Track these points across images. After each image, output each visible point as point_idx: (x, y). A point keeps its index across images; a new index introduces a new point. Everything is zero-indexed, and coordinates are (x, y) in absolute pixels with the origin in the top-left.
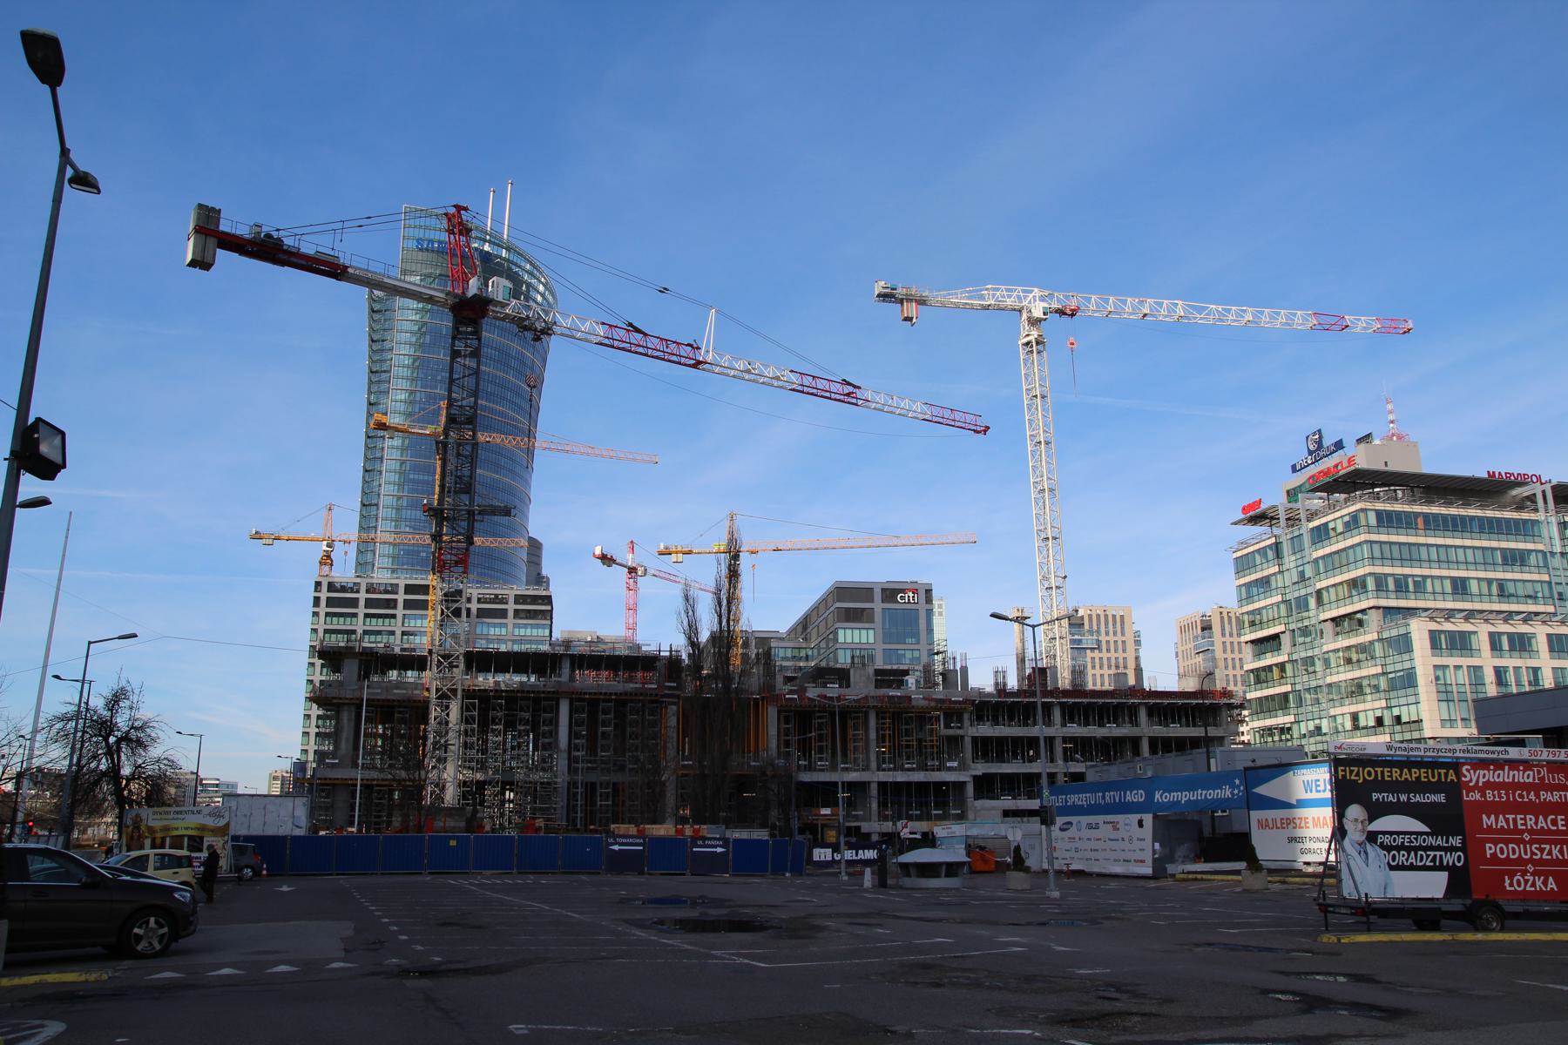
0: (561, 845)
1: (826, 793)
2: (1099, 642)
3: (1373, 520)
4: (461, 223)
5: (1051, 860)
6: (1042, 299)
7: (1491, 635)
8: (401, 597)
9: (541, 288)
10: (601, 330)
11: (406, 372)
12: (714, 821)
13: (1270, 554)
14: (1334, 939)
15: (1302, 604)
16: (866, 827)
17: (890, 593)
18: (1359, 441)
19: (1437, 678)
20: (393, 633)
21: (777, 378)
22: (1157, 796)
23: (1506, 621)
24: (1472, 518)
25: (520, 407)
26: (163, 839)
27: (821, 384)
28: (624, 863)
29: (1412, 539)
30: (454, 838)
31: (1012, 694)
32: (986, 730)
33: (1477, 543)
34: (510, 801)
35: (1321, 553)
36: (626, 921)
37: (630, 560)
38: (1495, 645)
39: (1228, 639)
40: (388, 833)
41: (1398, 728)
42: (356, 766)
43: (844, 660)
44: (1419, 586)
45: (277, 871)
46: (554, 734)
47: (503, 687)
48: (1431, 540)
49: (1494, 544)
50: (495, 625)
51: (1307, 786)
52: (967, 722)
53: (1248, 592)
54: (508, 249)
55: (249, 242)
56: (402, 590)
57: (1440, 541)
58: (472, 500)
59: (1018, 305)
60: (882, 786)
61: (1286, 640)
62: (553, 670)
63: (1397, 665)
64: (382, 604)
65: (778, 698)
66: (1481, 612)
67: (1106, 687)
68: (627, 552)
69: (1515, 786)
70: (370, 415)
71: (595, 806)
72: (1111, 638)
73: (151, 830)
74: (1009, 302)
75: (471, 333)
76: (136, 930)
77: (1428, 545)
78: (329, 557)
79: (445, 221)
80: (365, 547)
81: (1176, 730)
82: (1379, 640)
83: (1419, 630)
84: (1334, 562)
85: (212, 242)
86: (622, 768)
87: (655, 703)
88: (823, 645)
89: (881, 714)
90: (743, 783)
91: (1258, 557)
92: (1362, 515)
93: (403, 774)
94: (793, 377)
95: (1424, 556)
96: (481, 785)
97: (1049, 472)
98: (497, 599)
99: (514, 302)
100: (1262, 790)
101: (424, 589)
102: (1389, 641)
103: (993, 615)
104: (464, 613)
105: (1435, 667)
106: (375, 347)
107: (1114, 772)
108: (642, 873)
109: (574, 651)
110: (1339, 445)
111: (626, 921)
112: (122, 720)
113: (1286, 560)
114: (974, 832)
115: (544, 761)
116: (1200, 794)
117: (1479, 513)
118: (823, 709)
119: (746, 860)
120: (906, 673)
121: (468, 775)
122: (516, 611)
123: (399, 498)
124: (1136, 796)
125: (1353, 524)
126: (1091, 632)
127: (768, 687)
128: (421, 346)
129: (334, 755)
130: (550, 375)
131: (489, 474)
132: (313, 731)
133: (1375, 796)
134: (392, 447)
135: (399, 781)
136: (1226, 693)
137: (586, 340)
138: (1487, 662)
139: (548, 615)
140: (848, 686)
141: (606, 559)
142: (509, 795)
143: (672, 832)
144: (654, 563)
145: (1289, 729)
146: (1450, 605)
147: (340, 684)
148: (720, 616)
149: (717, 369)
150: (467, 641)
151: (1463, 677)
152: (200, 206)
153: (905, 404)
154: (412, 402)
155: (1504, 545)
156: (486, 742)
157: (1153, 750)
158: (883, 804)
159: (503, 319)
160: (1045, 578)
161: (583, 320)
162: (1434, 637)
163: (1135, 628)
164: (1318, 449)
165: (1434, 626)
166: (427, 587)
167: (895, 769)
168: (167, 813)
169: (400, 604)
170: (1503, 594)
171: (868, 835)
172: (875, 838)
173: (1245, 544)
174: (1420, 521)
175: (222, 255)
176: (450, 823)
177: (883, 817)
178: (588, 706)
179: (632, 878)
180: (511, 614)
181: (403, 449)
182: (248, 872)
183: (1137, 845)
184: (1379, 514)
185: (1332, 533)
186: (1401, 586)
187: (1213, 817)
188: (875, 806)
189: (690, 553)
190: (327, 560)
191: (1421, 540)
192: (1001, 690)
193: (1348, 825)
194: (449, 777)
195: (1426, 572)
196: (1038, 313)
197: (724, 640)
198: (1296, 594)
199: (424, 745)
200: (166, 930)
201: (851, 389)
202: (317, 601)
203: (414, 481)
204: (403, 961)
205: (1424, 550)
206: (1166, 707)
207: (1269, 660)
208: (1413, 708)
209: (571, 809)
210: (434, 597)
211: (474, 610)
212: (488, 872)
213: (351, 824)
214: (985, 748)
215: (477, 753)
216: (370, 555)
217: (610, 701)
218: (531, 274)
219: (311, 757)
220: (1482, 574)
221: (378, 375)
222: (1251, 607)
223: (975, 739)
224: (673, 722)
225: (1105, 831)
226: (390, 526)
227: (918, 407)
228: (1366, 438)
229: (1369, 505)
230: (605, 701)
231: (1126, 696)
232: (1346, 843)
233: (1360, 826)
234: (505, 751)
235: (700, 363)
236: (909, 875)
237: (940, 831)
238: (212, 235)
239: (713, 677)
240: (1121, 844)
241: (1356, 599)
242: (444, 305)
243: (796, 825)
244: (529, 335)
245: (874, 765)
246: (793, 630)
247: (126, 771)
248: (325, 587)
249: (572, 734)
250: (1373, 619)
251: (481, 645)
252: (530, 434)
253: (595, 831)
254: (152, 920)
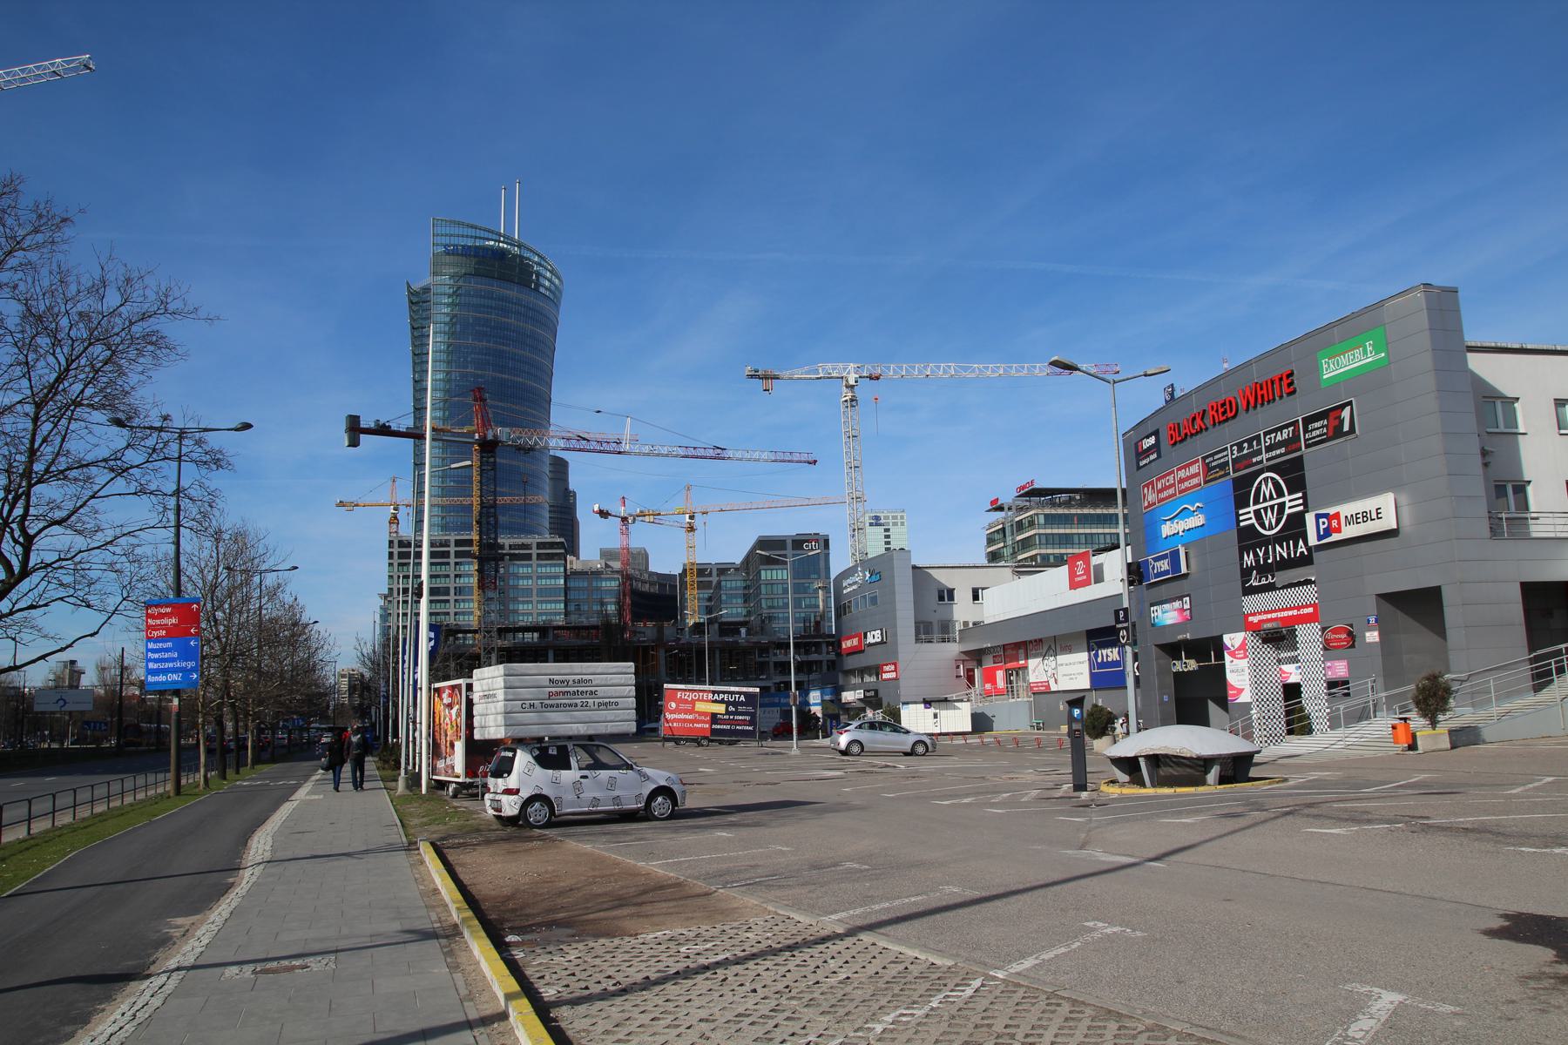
3: (1042, 520)
17: (799, 543)
37: (622, 512)
69: (685, 721)
89: (722, 651)
122: (539, 555)
128: (452, 334)
141: (604, 514)
154: (449, 381)
190: (394, 520)
196: (852, 382)
202: (391, 555)
218: (539, 264)
227: (765, 456)
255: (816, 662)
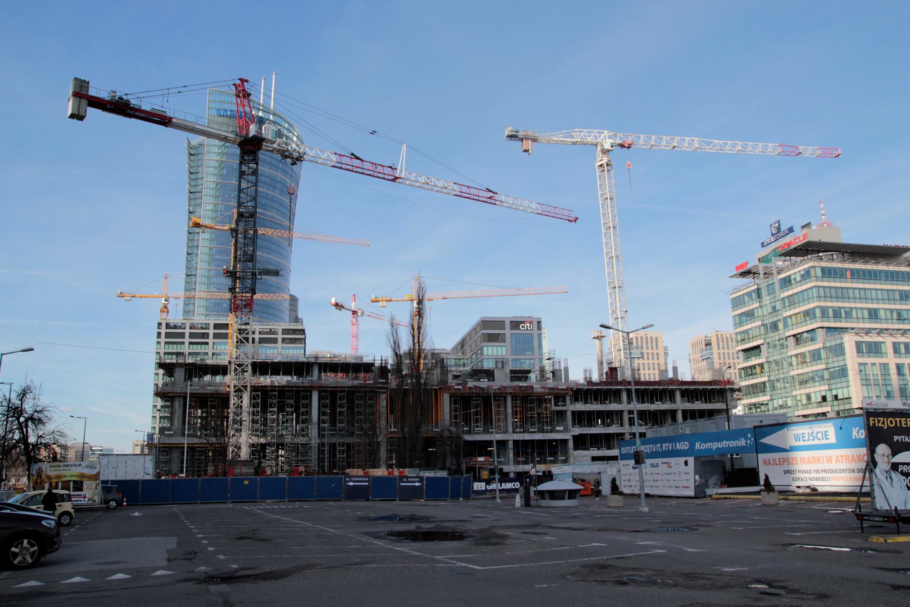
0: (318, 481)
1: (482, 448)
2: (642, 354)
3: (819, 273)
4: (244, 90)
5: (642, 488)
6: (610, 137)
7: (894, 344)
8: (211, 331)
9: (295, 139)
10: (334, 158)
11: (212, 192)
12: (411, 466)
13: (754, 296)
14: (882, 540)
15: (775, 327)
16: (506, 469)
17: (515, 324)
18: (803, 227)
19: (861, 371)
20: (207, 354)
21: (446, 188)
22: (697, 445)
23: (903, 335)
24: (881, 271)
25: (283, 213)
26: (57, 483)
27: (473, 191)
28: (357, 494)
29: (843, 285)
30: (247, 479)
31: (596, 384)
32: (580, 407)
33: (884, 287)
34: (282, 456)
35: (786, 294)
36: (367, 534)
38: (896, 350)
39: (721, 351)
40: (204, 477)
41: (836, 403)
42: (183, 435)
43: (488, 365)
44: (848, 314)
45: (134, 502)
46: (309, 413)
47: (276, 384)
48: (855, 285)
49: (895, 287)
50: (270, 348)
51: (797, 438)
52: (568, 402)
53: (740, 319)
54: (274, 115)
55: (108, 102)
56: (212, 327)
57: (861, 286)
58: (254, 266)
59: (595, 141)
60: (516, 442)
61: (764, 348)
62: (308, 373)
63: (835, 363)
64: (200, 336)
65: (449, 388)
66: (887, 330)
67: (657, 379)
68: (348, 305)
70: (190, 219)
71: (336, 459)
72: (650, 351)
73: (49, 478)
74: (589, 140)
75: (252, 160)
76: (13, 549)
77: (854, 289)
78: (166, 307)
79: (233, 88)
80: (189, 301)
81: (699, 405)
82: (824, 348)
83: (849, 341)
84: (792, 301)
85: (84, 102)
86: (352, 434)
87: (372, 393)
88: (474, 357)
89: (514, 397)
90: (430, 441)
91: (746, 298)
92: (812, 270)
93: (214, 440)
94: (456, 187)
95: (851, 295)
96: (264, 446)
97: (615, 245)
98: (271, 332)
99: (279, 140)
100: (767, 440)
101: (226, 326)
102: (830, 348)
103: (602, 326)
104: (250, 341)
105: (859, 364)
106: (193, 177)
107: (665, 431)
108: (368, 500)
109: (321, 361)
110: (791, 230)
111: (367, 534)
112: (28, 407)
113: (764, 299)
114: (578, 470)
115: (303, 430)
116: (724, 444)
117: (885, 268)
118: (478, 395)
119: (435, 491)
120: (529, 372)
121: (255, 440)
122: (283, 339)
123: (209, 270)
124: (683, 446)
125: (807, 275)
126: (637, 347)
127: (444, 382)
129: (169, 429)
130: (302, 174)
131: (265, 255)
132: (158, 415)
133: (896, 438)
134: (204, 238)
135: (211, 445)
136: (729, 382)
137: (326, 165)
138: (892, 360)
139: (303, 341)
140: (493, 380)
142: (281, 452)
143: (386, 473)
144: (368, 308)
145: (767, 404)
146: (867, 326)
147: (174, 384)
148: (413, 336)
149: (408, 182)
150: (253, 358)
151: (877, 371)
152: (76, 79)
153: (526, 203)
154: (216, 211)
155: (901, 288)
156: (266, 419)
157: (685, 418)
158: (516, 454)
159: (271, 151)
160: (614, 312)
161: (323, 152)
162: (858, 345)
163: (665, 344)
164: (778, 232)
165: (858, 339)
166: (228, 324)
167: (524, 432)
168: (59, 466)
169: (211, 336)
170: (900, 319)
171: (508, 474)
172: (512, 475)
173: (738, 289)
174: (848, 273)
175: (92, 112)
176: (244, 470)
177: (517, 463)
178: (330, 395)
179: (363, 503)
180: (280, 341)
181: (211, 240)
182: (113, 504)
183: (684, 477)
184: (823, 269)
185: (793, 282)
186: (837, 314)
187: (732, 458)
188: (511, 455)
189: (390, 301)
191: (849, 285)
192: (590, 383)
193: (878, 458)
194: (243, 441)
195: (852, 305)
196: (607, 146)
197: (416, 354)
198: (771, 320)
199: (227, 422)
200: (36, 548)
201: (491, 194)
202: (159, 334)
203: (216, 260)
204: (210, 569)
205: (850, 291)
206: (693, 391)
207: (753, 361)
208: (845, 390)
209: (321, 460)
210: (232, 331)
211: (257, 340)
212: (269, 501)
213: (182, 472)
214: (581, 418)
215: (261, 425)
216: (191, 306)
217: (344, 391)
218: (288, 130)
219: (157, 431)
220: (887, 306)
221: (194, 194)
222: (742, 329)
223: (573, 413)
224: (384, 403)
225: (663, 468)
226: (204, 288)
228: (808, 225)
229: (816, 264)
230: (341, 392)
231: (667, 384)
232: (877, 471)
233: (886, 459)
234: (278, 424)
235: (397, 178)
236: (544, 498)
237: (555, 469)
238: (85, 99)
239: (411, 376)
240: (675, 477)
241: (808, 322)
242: (234, 142)
243: (464, 468)
244: (289, 161)
245: (510, 429)
246: (455, 348)
247: (32, 439)
248: (164, 326)
249: (320, 413)
250: (820, 334)
251: (261, 358)
252: (290, 229)
253: (337, 474)
254: (26, 541)
255: (617, 412)
